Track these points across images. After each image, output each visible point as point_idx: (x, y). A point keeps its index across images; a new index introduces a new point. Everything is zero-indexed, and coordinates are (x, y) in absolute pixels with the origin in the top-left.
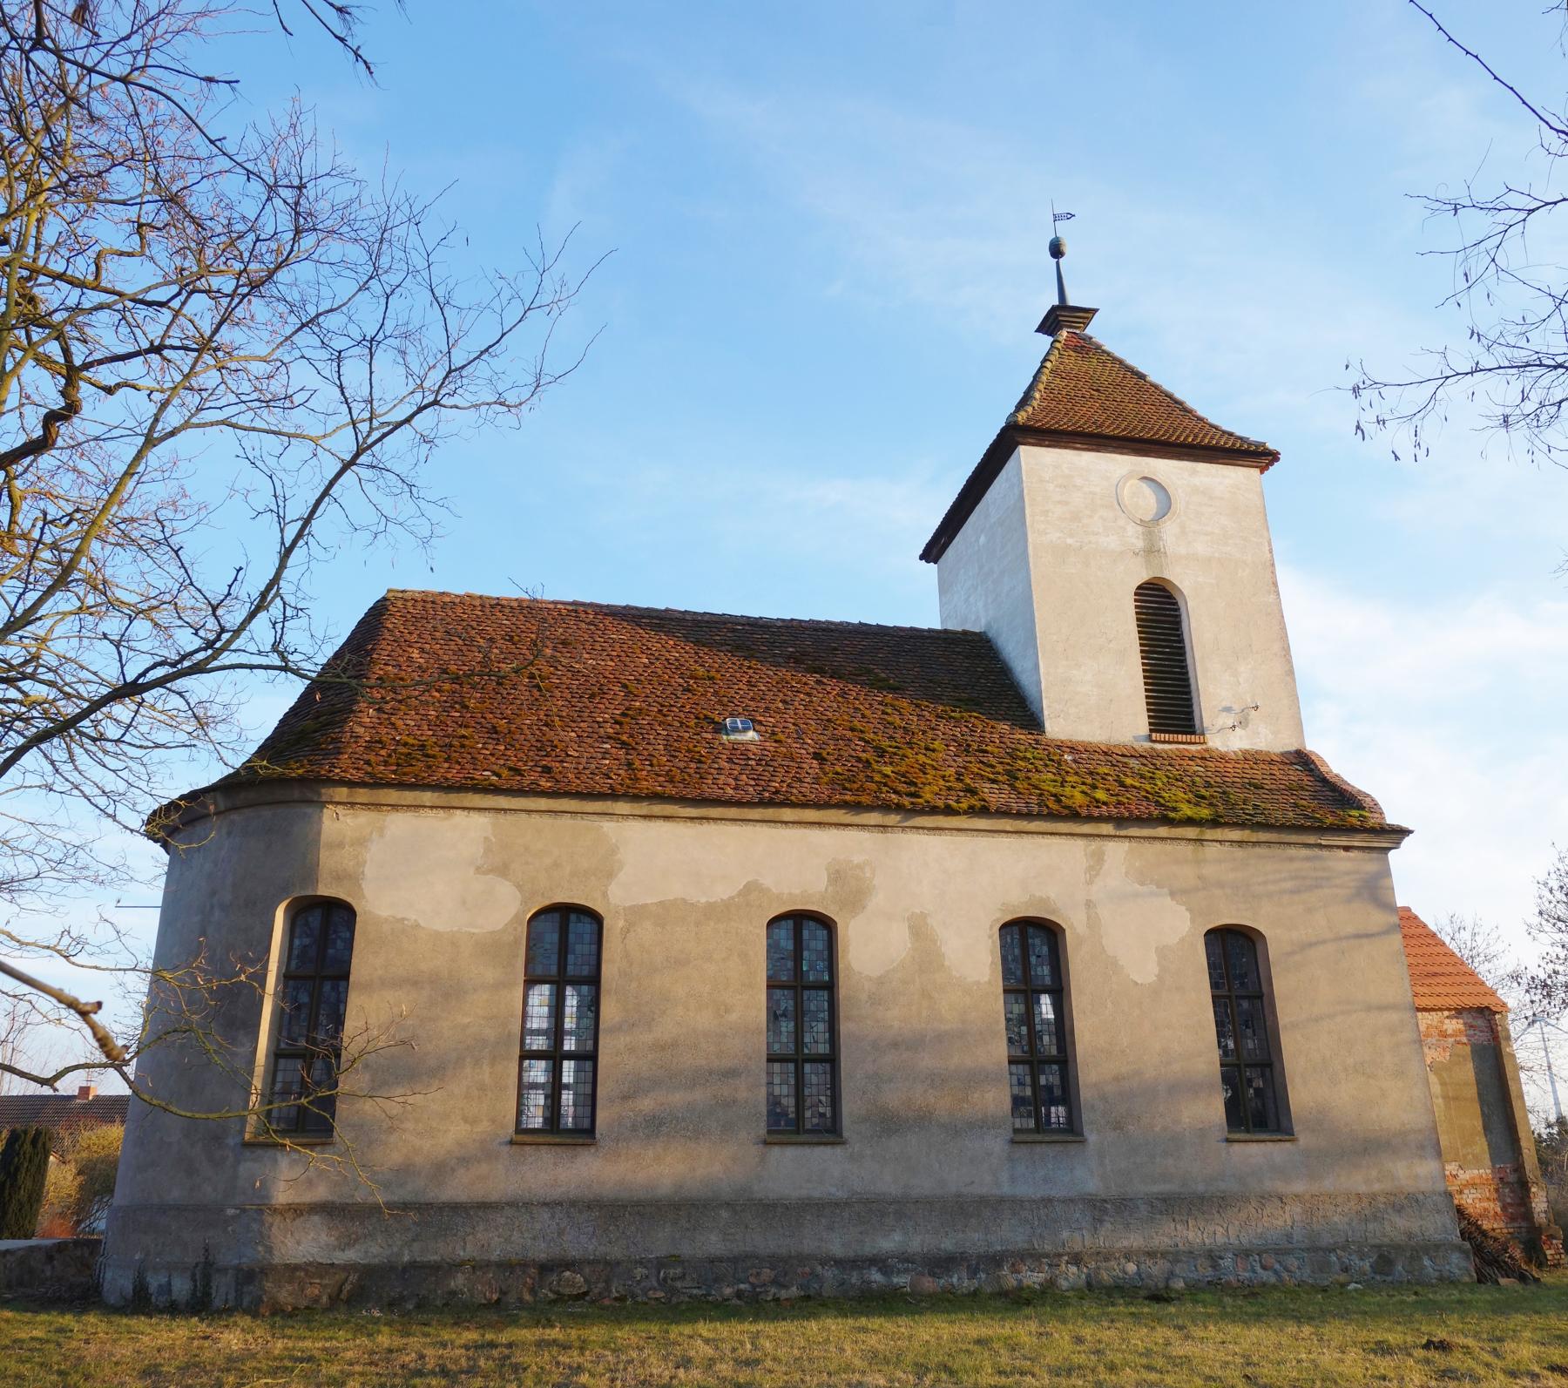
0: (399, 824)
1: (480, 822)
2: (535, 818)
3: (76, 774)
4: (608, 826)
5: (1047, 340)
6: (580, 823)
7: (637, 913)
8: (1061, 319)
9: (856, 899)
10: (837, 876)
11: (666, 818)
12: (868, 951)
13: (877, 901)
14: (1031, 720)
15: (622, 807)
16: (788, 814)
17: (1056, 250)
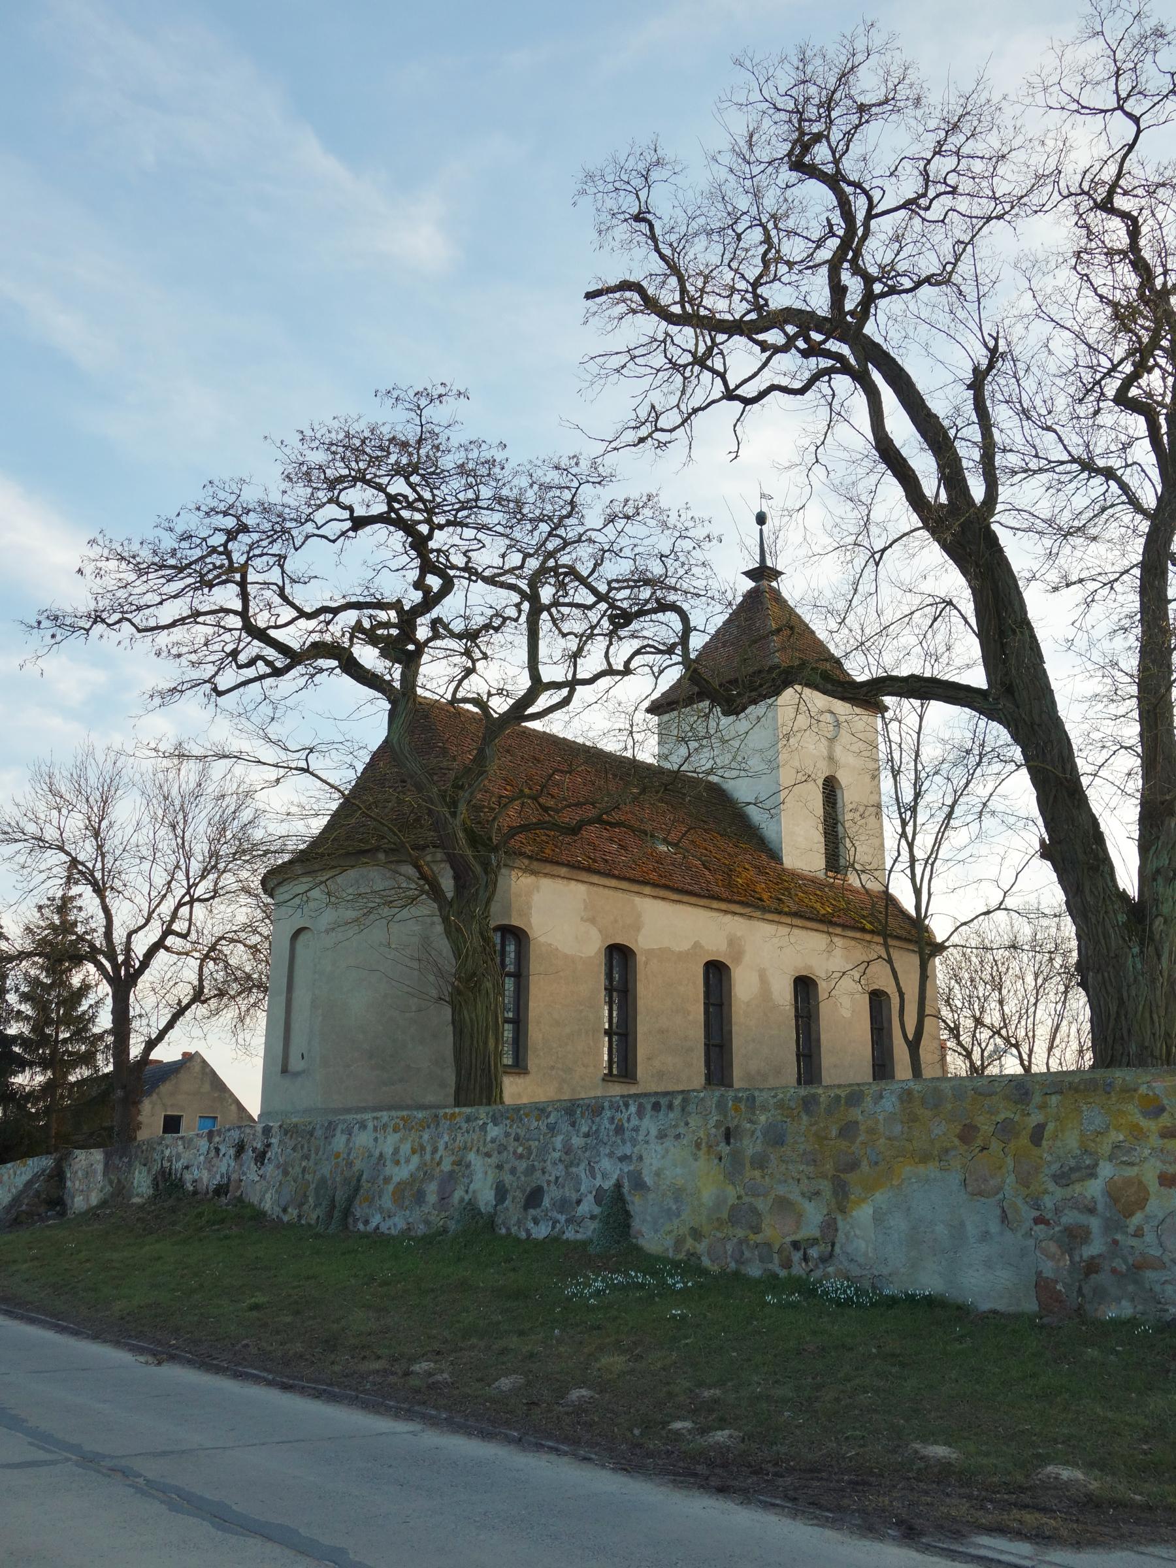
0: (545, 883)
1: (582, 888)
2: (606, 891)
3: (902, 851)
4: (637, 900)
5: (750, 584)
6: (626, 896)
7: (650, 952)
8: (763, 573)
9: (738, 956)
10: (732, 942)
11: (663, 899)
12: (744, 986)
13: (747, 959)
14: (782, 864)
15: (647, 890)
16: (715, 904)
17: (761, 519)
